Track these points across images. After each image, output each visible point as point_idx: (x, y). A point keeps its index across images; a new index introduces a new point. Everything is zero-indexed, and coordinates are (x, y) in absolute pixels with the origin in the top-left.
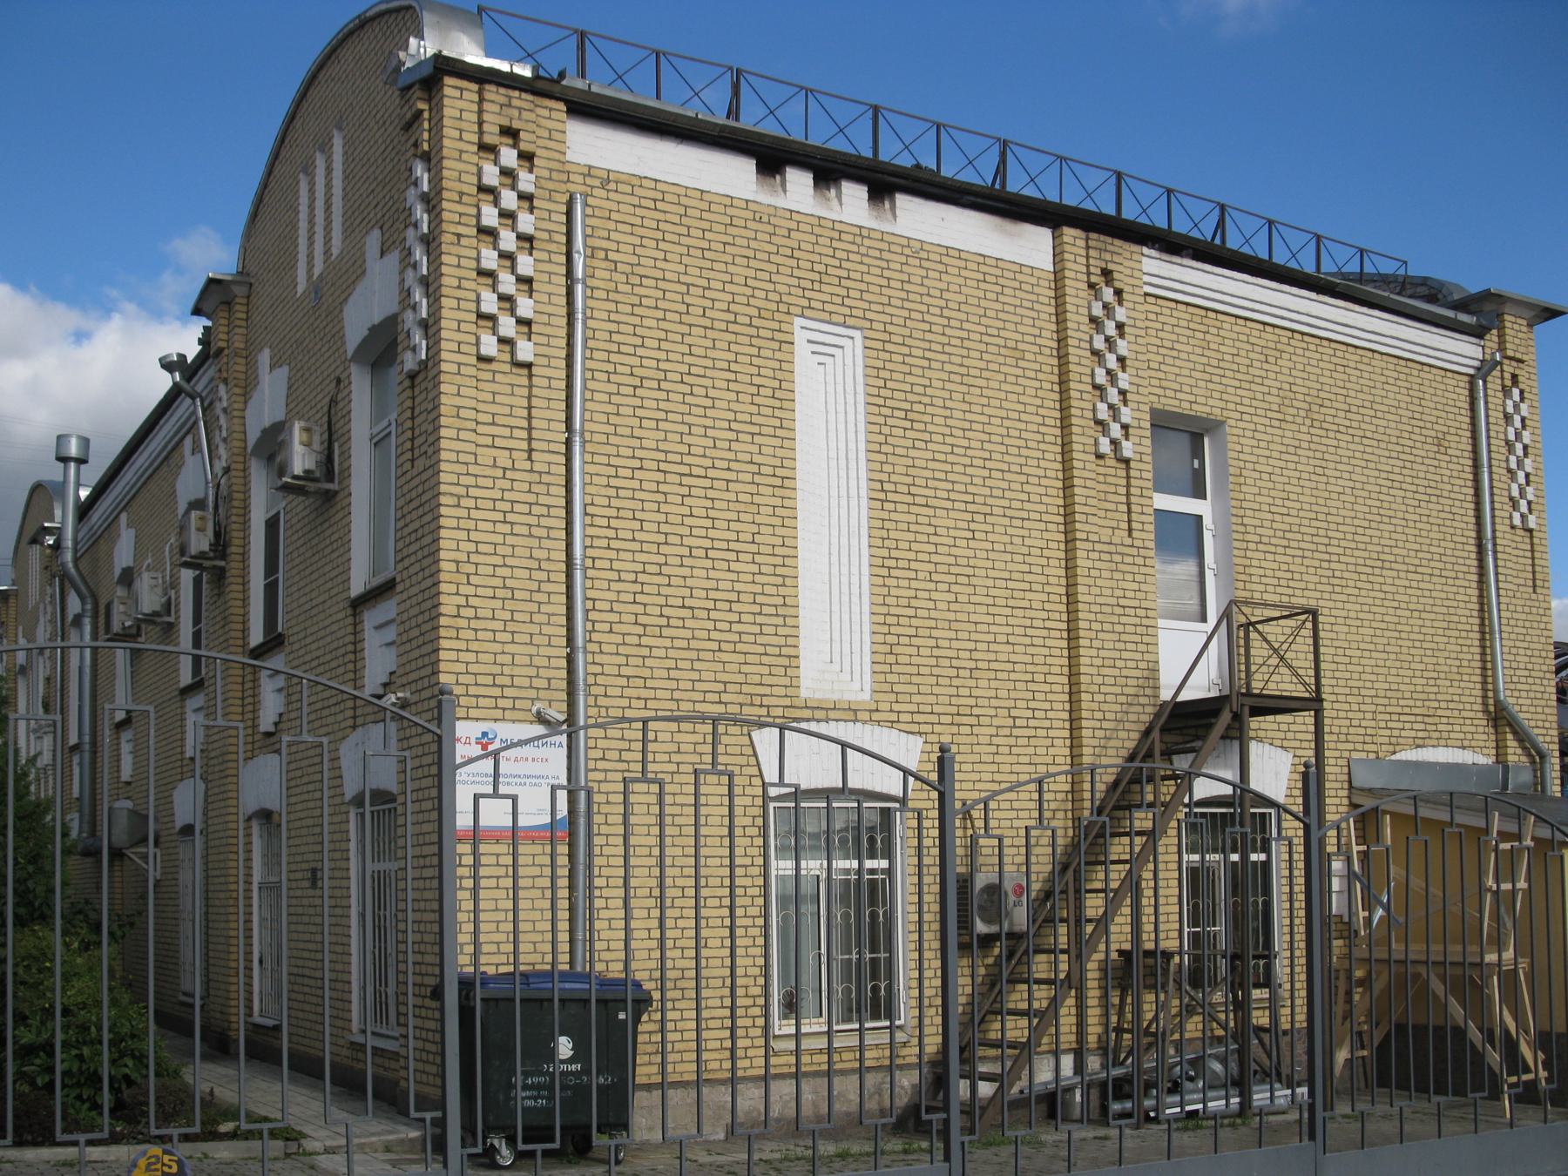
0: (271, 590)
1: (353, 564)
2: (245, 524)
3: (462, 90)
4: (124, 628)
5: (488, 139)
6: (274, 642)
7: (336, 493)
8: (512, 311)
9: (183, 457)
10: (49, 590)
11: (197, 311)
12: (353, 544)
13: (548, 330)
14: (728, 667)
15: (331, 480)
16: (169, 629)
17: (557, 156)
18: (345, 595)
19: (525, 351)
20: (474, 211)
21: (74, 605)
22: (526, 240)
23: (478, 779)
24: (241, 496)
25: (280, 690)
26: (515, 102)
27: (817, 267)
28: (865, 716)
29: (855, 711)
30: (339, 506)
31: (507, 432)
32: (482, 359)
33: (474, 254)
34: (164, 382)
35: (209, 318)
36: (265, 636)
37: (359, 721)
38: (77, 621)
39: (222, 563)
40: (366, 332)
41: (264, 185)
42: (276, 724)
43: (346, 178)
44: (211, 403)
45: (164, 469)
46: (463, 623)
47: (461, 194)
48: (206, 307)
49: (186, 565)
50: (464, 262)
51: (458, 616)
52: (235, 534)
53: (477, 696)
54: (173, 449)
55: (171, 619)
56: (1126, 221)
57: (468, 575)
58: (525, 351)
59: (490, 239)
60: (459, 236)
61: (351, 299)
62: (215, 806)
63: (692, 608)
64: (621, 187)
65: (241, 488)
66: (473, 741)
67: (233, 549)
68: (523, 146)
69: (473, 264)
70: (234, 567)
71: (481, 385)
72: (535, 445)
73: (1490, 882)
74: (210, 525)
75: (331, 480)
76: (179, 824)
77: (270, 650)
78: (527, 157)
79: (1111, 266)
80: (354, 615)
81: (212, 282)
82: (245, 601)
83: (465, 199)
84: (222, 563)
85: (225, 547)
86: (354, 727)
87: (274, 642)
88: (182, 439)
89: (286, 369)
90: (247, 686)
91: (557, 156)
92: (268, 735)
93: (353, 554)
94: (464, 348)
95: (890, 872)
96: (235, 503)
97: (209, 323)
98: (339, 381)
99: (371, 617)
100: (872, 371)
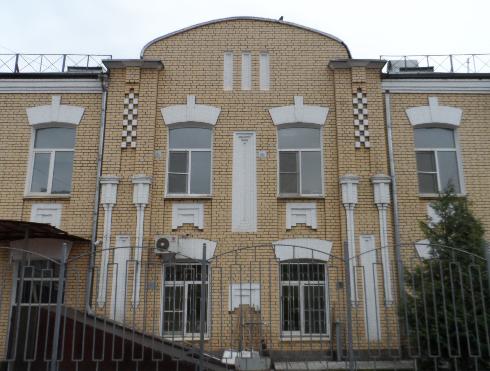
5: (354, 92)
78: (365, 95)
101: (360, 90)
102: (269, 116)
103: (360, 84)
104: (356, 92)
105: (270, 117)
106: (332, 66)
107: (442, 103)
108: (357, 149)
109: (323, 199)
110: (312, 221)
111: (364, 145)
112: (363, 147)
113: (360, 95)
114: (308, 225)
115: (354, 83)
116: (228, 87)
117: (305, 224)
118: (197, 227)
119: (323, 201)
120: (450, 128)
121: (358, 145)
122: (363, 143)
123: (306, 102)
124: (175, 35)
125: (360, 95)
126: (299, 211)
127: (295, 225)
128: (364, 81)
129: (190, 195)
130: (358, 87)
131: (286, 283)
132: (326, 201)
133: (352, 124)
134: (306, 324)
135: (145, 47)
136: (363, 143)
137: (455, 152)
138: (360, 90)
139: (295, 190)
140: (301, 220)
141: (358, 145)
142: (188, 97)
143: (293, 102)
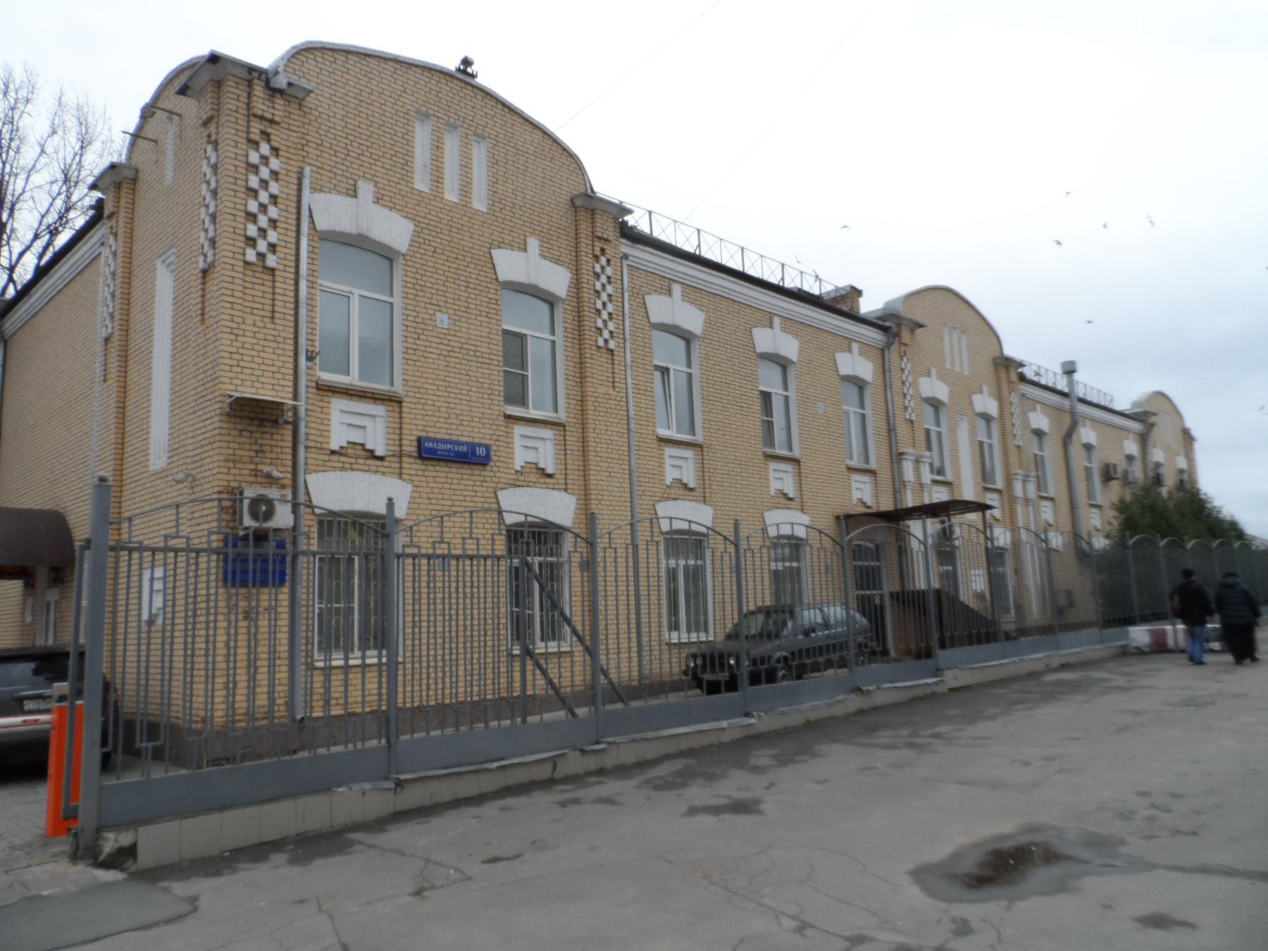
5: (253, 137)
8: (267, 165)
13: (286, 178)
14: (344, 145)
19: (271, 261)
20: (244, 178)
22: (274, 198)
27: (465, 351)
31: (260, 306)
32: (246, 263)
33: (242, 226)
35: (103, 193)
48: (100, 184)
56: (701, 308)
58: (271, 261)
59: (255, 146)
62: (136, 527)
68: (274, 144)
69: (243, 183)
71: (247, 291)
72: (276, 309)
73: (664, 562)
78: (275, 150)
101: (266, 136)
102: (489, 260)
103: (268, 124)
104: (256, 138)
105: (493, 264)
106: (578, 202)
107: (686, 298)
108: (247, 263)
109: (563, 425)
110: (547, 456)
111: (264, 261)
112: (260, 263)
113: (265, 149)
114: (369, 446)
115: (255, 116)
116: (421, 183)
117: (536, 464)
118: (543, 470)
119: (562, 428)
120: (387, 255)
121: (251, 255)
122: (261, 256)
123: (378, 200)
124: (555, 141)
125: (265, 149)
126: (529, 440)
127: (345, 444)
128: (277, 119)
129: (533, 413)
130: (262, 128)
131: (855, 563)
132: (404, 404)
133: (243, 208)
134: (688, 621)
135: (293, 48)
136: (261, 256)
137: (392, 304)
138: (266, 136)
139: (523, 402)
140: (357, 437)
141: (251, 255)
142: (360, 184)
143: (353, 193)
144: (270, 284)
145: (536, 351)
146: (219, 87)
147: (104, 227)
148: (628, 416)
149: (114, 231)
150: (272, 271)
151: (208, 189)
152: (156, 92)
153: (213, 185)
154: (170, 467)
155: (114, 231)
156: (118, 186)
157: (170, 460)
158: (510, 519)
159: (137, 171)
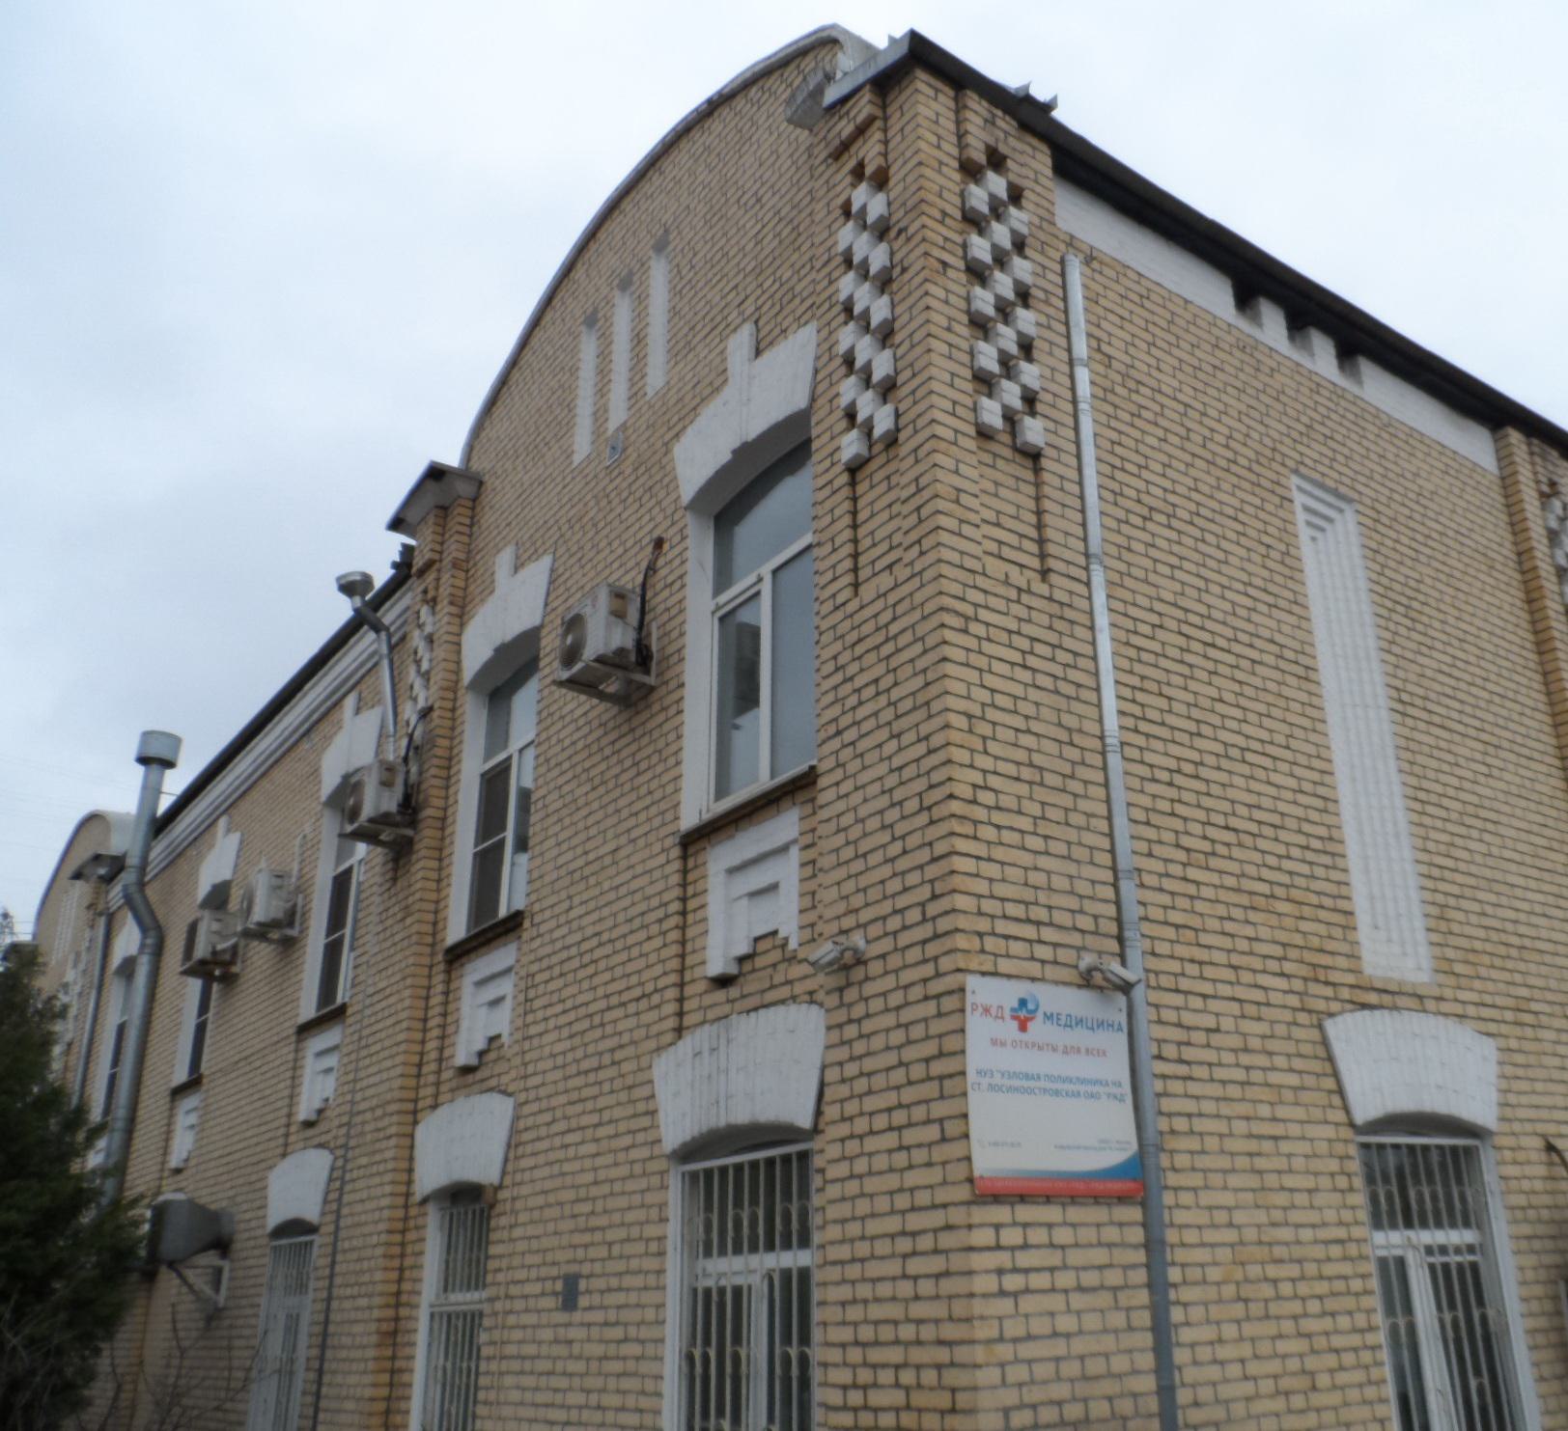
0: (332, 952)
1: (686, 784)
2: (448, 780)
3: (937, 90)
4: (214, 953)
6: (194, 1083)
7: (652, 689)
9: (340, 721)
10: (87, 934)
11: (397, 524)
12: (686, 755)
15: (647, 672)
16: (289, 945)
17: (1046, 204)
18: (671, 828)
21: (128, 940)
23: (1016, 1083)
24: (445, 743)
25: (192, 1127)
26: (1000, 123)
28: (1431, 1005)
29: (1420, 997)
30: (656, 707)
34: (343, 610)
35: (412, 535)
36: (468, 929)
37: (688, 1020)
38: (128, 968)
39: (409, 832)
40: (725, 457)
41: (514, 363)
42: (481, 1054)
43: (570, 408)
44: (403, 638)
45: (305, 745)
46: (980, 813)
47: (944, 214)
48: (412, 517)
49: (359, 835)
50: (953, 299)
51: (974, 802)
52: (433, 792)
53: (1007, 937)
54: (370, 670)
55: (294, 932)
57: (984, 738)
60: (945, 264)
61: (689, 430)
63: (1178, 846)
64: (1106, 271)
65: (448, 733)
66: (1007, 1013)
67: (428, 812)
70: (426, 837)
74: (399, 780)
75: (647, 672)
76: (275, 1217)
77: (474, 949)
79: (1556, 478)
80: (684, 857)
81: (435, 473)
82: (441, 881)
83: (948, 221)
84: (409, 832)
85: (416, 811)
86: (284, 1155)
87: (331, 1015)
88: (338, 704)
89: (546, 561)
90: (434, 1001)
91: (1046, 204)
92: (467, 1070)
93: (686, 768)
94: (959, 410)
95: (1481, 1248)
96: (438, 752)
97: (412, 542)
98: (659, 543)
99: (720, 857)
100: (1372, 553)
108: (984, 434)
121: (991, 414)
144: (1031, 490)
145: (477, 977)
146: (445, 517)
147: (410, 595)
148: (1119, 920)
149: (430, 596)
150: (1033, 456)
151: (418, 671)
152: (663, 140)
153: (425, 666)
154: (1335, 1006)
155: (430, 596)
156: (444, 510)
157: (835, 1036)
158: (1365, 1110)
159: (481, 483)
